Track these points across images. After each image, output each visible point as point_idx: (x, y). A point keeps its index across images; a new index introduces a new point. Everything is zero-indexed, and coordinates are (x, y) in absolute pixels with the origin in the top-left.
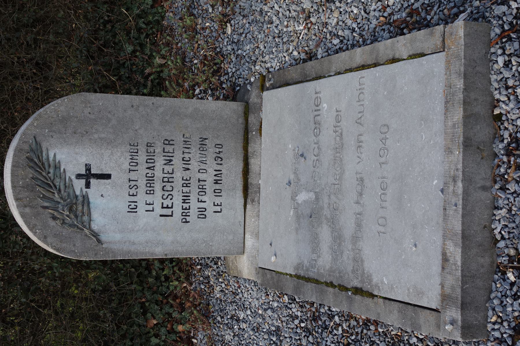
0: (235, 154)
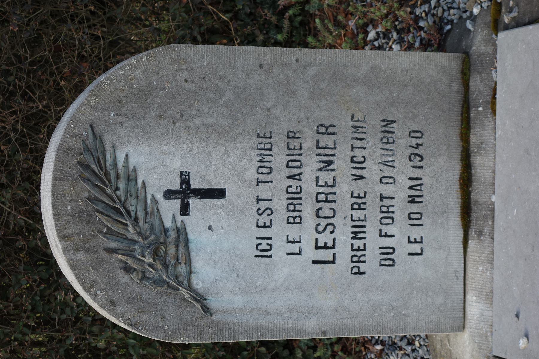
0: (445, 148)
